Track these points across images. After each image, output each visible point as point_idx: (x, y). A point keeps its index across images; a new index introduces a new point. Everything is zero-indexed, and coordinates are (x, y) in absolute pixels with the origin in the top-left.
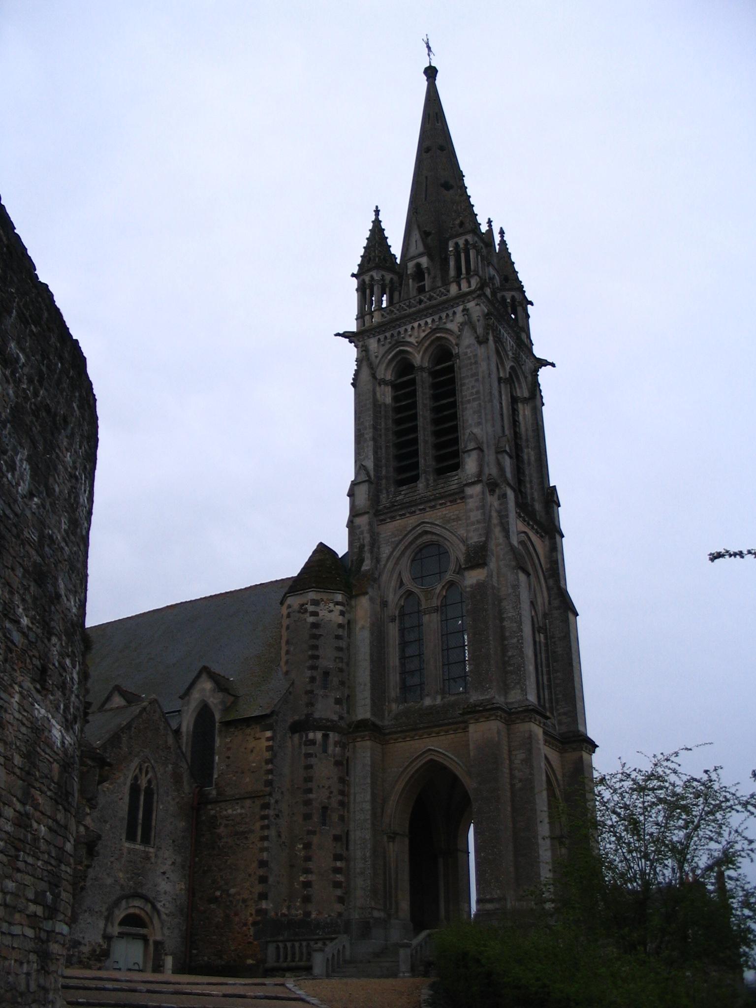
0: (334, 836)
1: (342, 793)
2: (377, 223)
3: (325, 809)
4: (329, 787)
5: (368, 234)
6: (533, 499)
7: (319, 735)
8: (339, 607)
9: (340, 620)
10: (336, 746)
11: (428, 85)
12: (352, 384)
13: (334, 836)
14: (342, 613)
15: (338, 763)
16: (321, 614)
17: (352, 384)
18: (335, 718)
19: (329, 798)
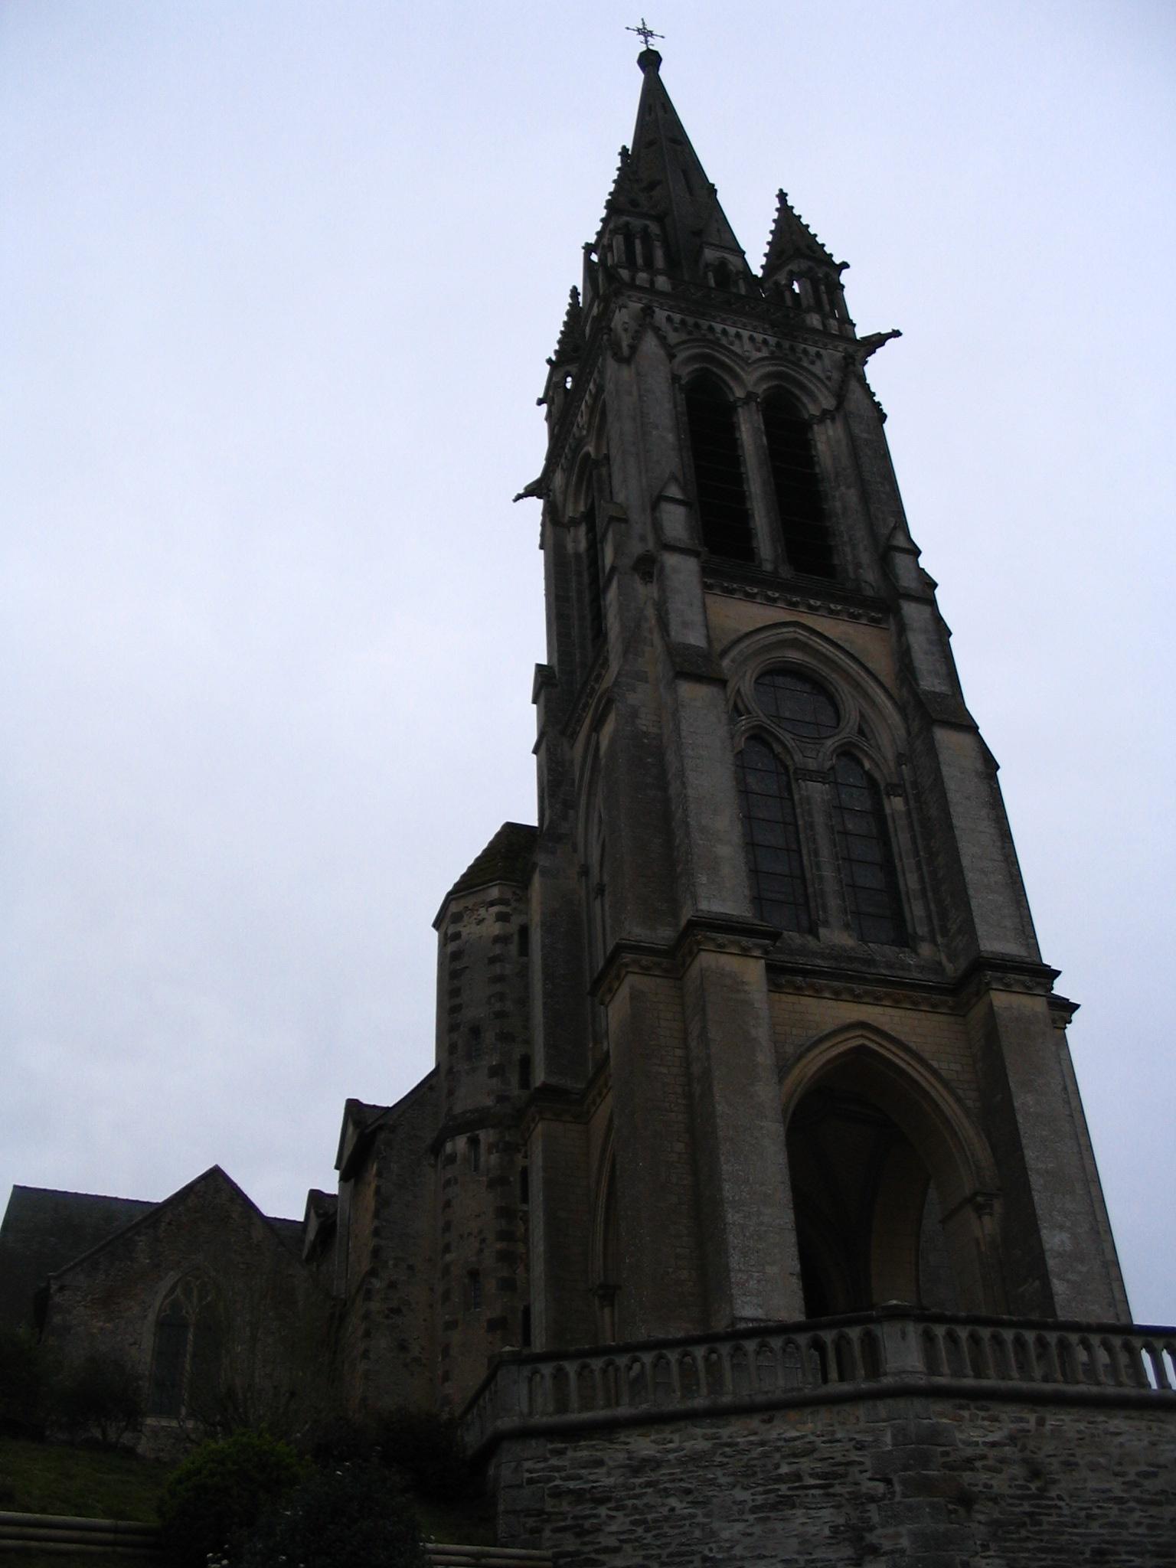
0: (489, 1321)
1: (505, 1236)
2: (657, 114)
3: (474, 1275)
4: (481, 1232)
5: (615, 175)
6: (858, 566)
7: (461, 1143)
8: (495, 909)
9: (496, 929)
10: (490, 1152)
11: (646, 79)
12: (935, 585)
13: (489, 1321)
14: (502, 917)
15: (498, 1182)
16: (465, 932)
17: (935, 585)
18: (489, 1102)
19: (481, 1251)
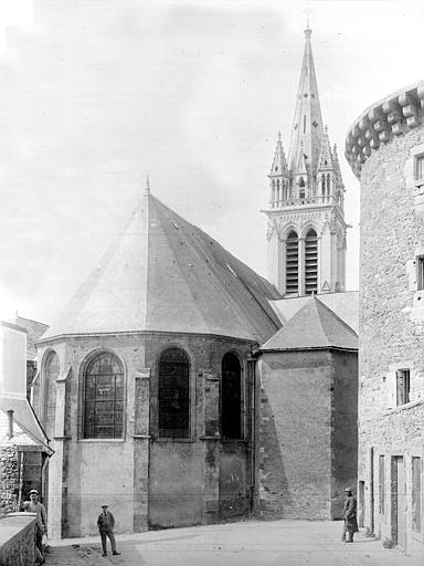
2: (280, 143)
